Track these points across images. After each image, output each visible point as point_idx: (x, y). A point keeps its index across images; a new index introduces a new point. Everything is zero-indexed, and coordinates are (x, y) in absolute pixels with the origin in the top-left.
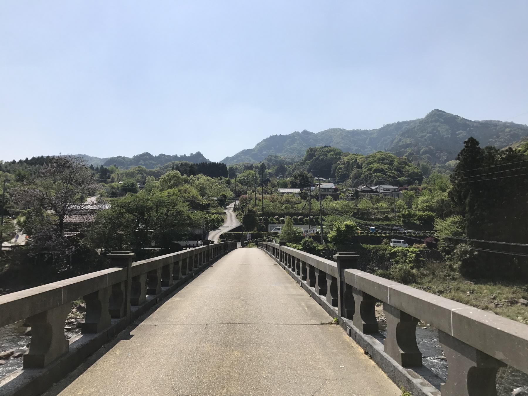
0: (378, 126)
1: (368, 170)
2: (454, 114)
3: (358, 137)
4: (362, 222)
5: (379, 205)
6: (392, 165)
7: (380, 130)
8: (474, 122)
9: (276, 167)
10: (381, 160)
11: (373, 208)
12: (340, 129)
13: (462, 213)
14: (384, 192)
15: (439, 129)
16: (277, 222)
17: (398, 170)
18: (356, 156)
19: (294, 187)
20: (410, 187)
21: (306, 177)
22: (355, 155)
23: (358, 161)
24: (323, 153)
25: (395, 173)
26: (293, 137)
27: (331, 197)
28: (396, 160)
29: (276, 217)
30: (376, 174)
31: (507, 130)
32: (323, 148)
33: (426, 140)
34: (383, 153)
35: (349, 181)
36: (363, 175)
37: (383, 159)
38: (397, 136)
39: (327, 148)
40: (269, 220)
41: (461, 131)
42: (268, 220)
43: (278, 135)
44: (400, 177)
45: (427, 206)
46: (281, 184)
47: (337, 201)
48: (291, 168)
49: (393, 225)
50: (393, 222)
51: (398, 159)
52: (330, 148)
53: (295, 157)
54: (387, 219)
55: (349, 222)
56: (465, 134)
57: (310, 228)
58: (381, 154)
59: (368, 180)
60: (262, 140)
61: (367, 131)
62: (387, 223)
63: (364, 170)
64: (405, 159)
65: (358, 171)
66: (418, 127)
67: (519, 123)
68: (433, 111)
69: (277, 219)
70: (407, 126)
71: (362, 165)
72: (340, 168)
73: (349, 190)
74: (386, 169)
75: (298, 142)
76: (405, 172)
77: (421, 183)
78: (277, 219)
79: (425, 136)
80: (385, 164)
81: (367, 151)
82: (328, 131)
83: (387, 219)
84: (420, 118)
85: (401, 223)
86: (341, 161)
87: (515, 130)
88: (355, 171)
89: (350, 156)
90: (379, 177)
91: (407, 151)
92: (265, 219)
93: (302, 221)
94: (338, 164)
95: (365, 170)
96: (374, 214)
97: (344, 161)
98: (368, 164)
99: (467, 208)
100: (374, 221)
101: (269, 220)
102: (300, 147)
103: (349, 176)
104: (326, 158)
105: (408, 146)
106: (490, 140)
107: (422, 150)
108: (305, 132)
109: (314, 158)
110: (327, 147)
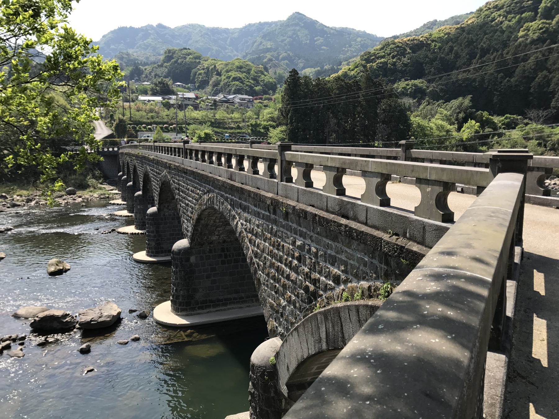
0: (240, 25)
1: (227, 78)
2: (314, 19)
3: (219, 36)
4: (218, 130)
5: (233, 116)
6: (249, 74)
7: (241, 30)
8: (332, 29)
9: (130, 68)
10: (240, 68)
11: (228, 118)
12: (199, 25)
13: (287, 125)
14: (240, 101)
15: (299, 33)
16: (145, 130)
17: (255, 79)
18: (216, 62)
19: (154, 94)
20: (264, 96)
21: (167, 84)
22: (215, 60)
23: (218, 67)
24: (182, 56)
25: (252, 82)
26: (146, 31)
27: (192, 108)
28: (253, 69)
29: (144, 125)
30: (234, 83)
31: (359, 39)
32: (181, 50)
33: (286, 45)
34: (241, 61)
35: (209, 89)
36: (222, 83)
37: (241, 67)
38: (258, 38)
39: (186, 51)
40: (138, 129)
41: (319, 37)
42: (136, 128)
43: (128, 27)
44: (256, 87)
45: (270, 117)
46: (141, 91)
47: (198, 112)
48: (147, 70)
49: (244, 133)
50: (243, 131)
51: (255, 67)
52: (189, 51)
53: (150, 56)
54: (239, 127)
55: (207, 131)
56: (322, 41)
57: (177, 135)
58: (239, 61)
59: (226, 89)
60: (109, 31)
61: (227, 29)
62: (239, 131)
63: (223, 77)
64: (262, 68)
65: (217, 78)
66: (279, 30)
67: (370, 33)
68: (294, 14)
69: (145, 127)
70: (268, 27)
71: (221, 72)
72: (200, 74)
73: (208, 99)
74: (244, 78)
75: (152, 36)
76: (261, 81)
77: (275, 92)
78: (145, 127)
79: (285, 40)
80: (243, 72)
81: (228, 52)
82: (186, 27)
83: (239, 127)
84: (281, 19)
85: (249, 131)
86: (200, 66)
87: (365, 40)
88: (214, 78)
89: (209, 60)
90: (237, 86)
91: (266, 57)
92: (133, 128)
93: (168, 129)
94: (198, 69)
95: (225, 77)
96: (229, 124)
97: (204, 66)
98: (227, 71)
99: (289, 121)
100: (228, 129)
101: (138, 129)
102: (155, 44)
103: (209, 82)
104: (185, 62)
105: (268, 50)
106: (344, 49)
107: (281, 56)
108: (160, 26)
109: (173, 60)
110: (186, 49)
